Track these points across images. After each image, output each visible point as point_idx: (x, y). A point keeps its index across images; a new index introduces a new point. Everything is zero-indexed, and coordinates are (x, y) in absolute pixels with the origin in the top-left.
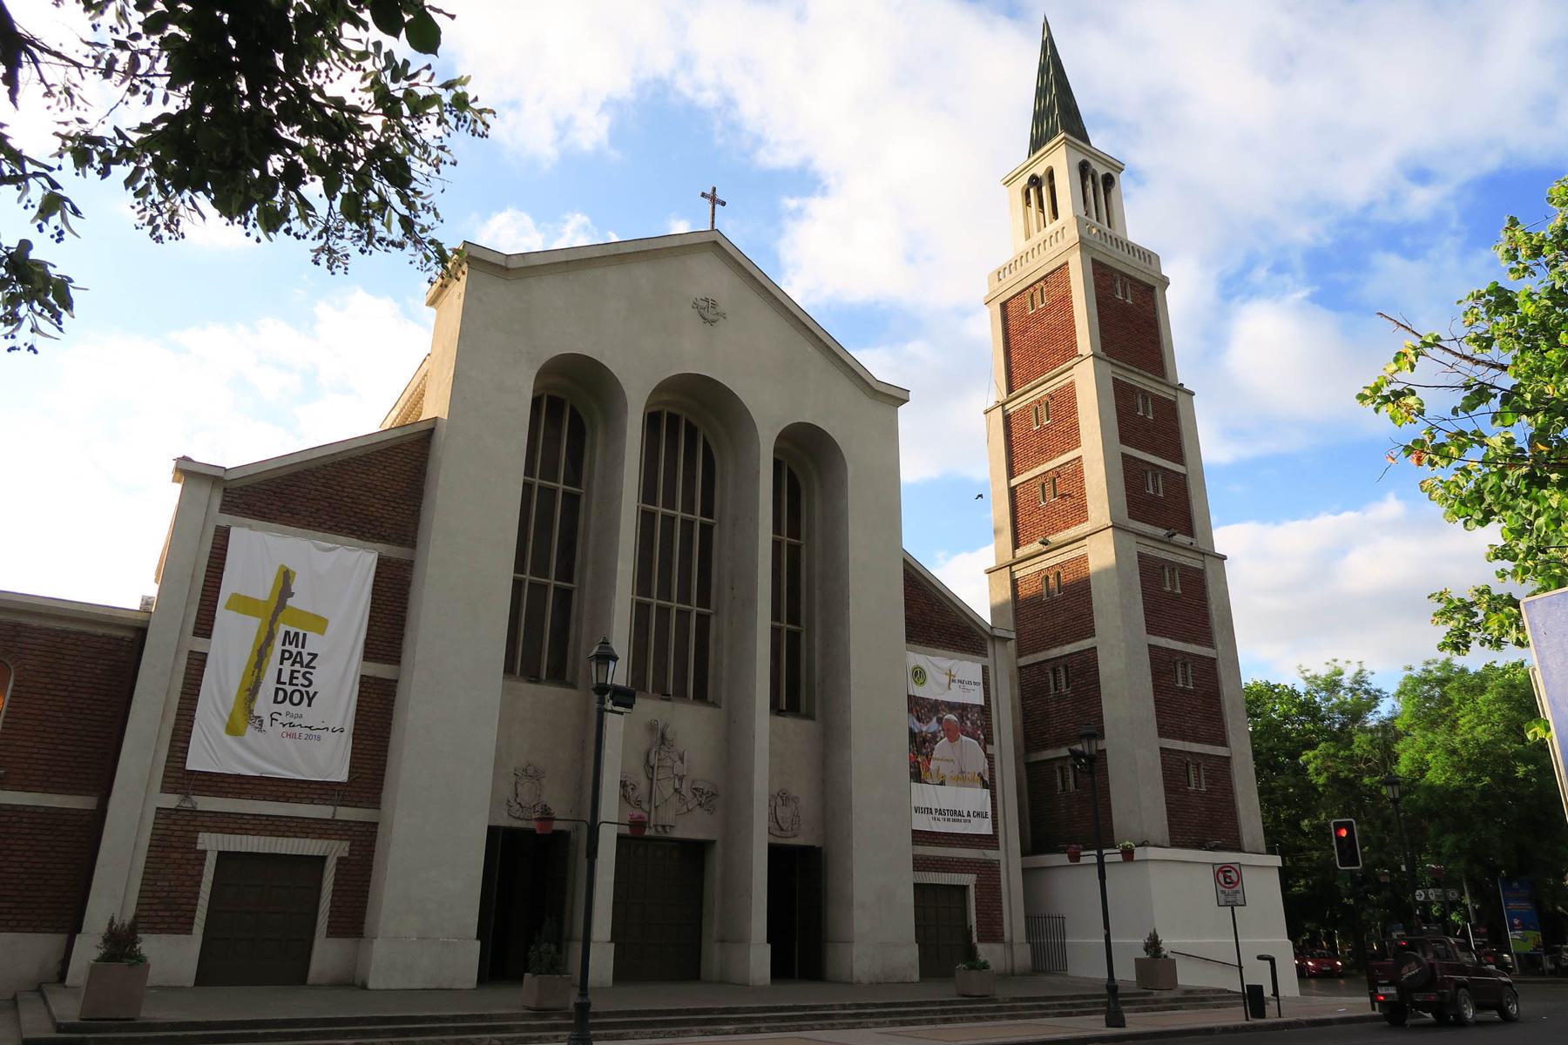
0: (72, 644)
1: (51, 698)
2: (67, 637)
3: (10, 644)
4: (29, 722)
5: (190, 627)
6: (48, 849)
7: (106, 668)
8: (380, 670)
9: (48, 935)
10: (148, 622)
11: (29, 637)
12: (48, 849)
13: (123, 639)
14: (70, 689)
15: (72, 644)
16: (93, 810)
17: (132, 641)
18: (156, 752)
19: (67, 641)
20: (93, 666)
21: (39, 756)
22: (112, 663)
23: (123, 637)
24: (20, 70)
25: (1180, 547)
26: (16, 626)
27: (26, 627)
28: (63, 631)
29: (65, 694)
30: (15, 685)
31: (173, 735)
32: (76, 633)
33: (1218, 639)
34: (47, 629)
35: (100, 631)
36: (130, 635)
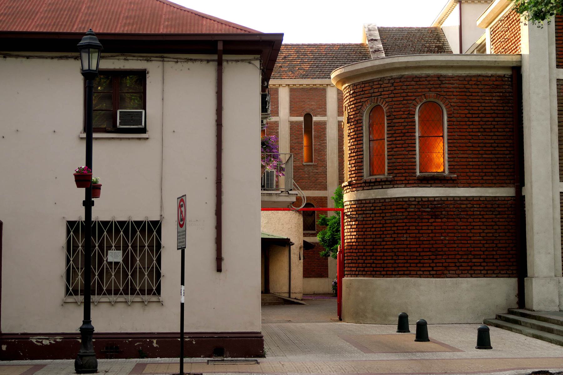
0: (475, 84)
1: (471, 123)
2: (471, 80)
3: (439, 89)
4: (463, 141)
5: (554, 63)
6: (493, 223)
7: (499, 98)
8: (220, 46)
9: (505, 279)
10: (521, 62)
11: (449, 84)
12: (493, 223)
13: (504, 76)
14: (480, 115)
15: (475, 84)
16: (514, 197)
17: (511, 76)
18: (552, 154)
19: (471, 83)
20: (490, 98)
21: (474, 163)
22: (501, 94)
23: (505, 75)
24: (84, 199)
25: (63, 57)
26: (439, 77)
27: (445, 77)
28: (467, 76)
29: (479, 119)
30: (448, 117)
31: (559, 141)
32: (474, 76)
33: (216, 38)
34: (457, 76)
35: (490, 72)
36: (509, 73)
